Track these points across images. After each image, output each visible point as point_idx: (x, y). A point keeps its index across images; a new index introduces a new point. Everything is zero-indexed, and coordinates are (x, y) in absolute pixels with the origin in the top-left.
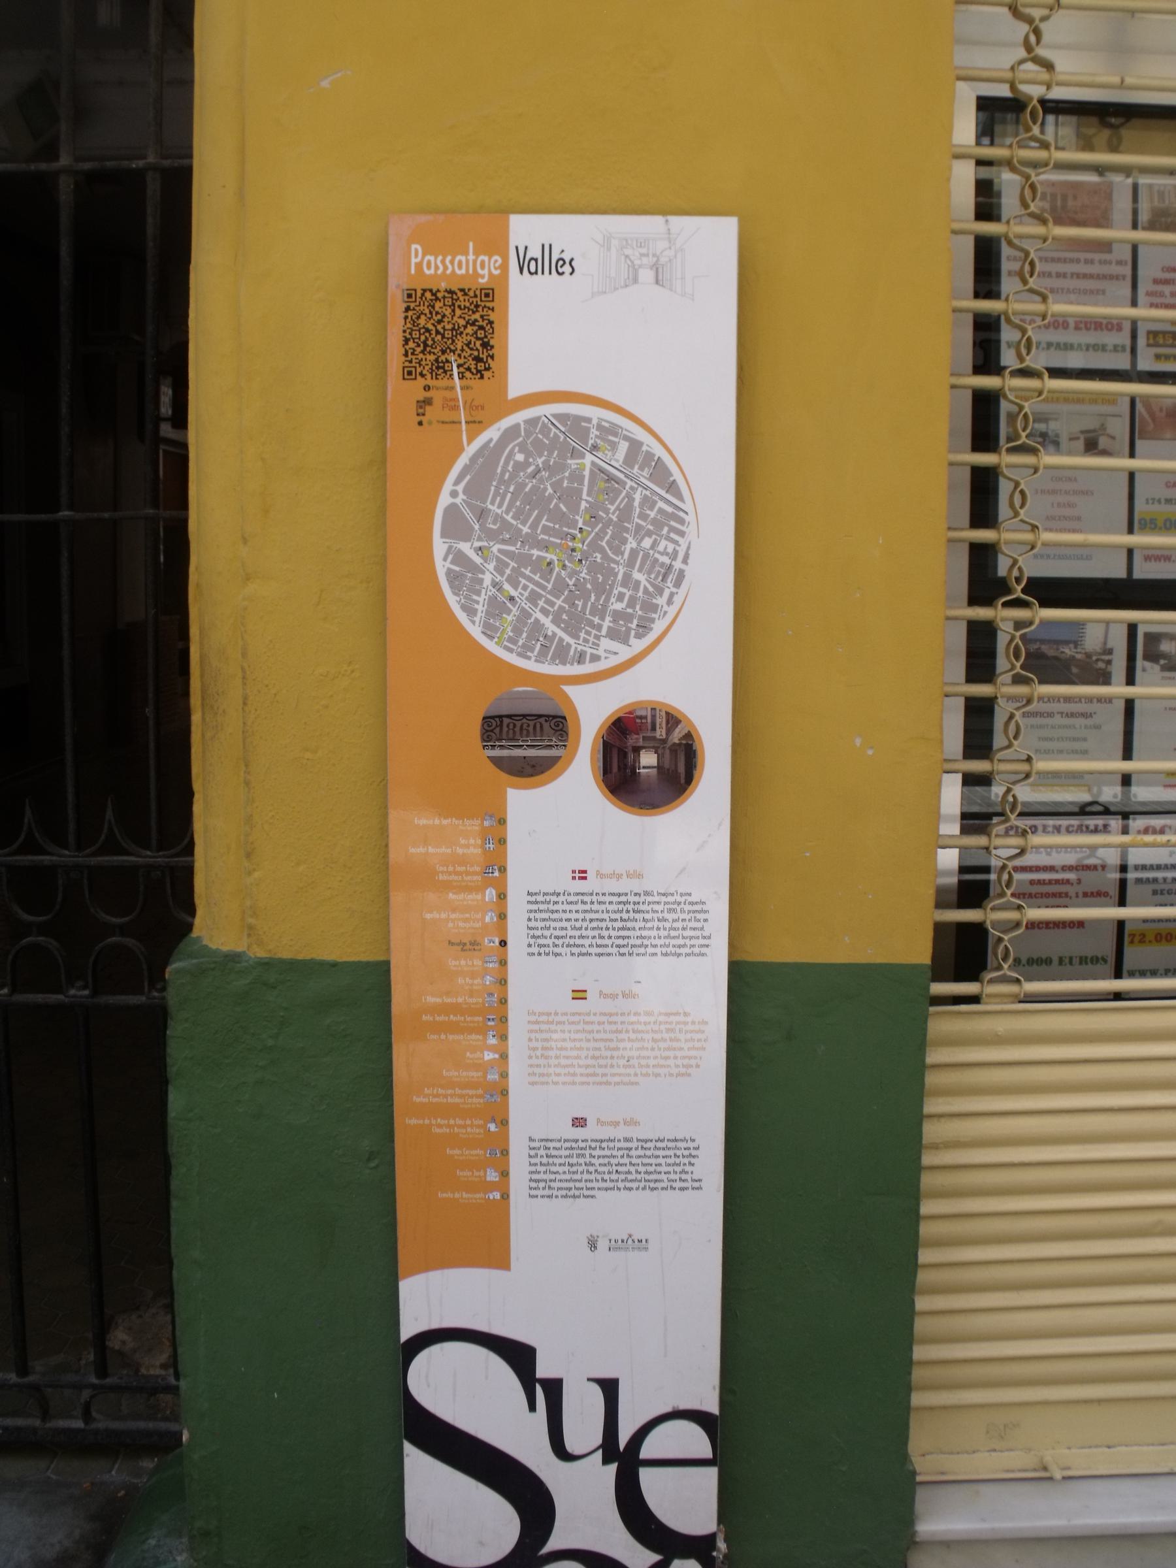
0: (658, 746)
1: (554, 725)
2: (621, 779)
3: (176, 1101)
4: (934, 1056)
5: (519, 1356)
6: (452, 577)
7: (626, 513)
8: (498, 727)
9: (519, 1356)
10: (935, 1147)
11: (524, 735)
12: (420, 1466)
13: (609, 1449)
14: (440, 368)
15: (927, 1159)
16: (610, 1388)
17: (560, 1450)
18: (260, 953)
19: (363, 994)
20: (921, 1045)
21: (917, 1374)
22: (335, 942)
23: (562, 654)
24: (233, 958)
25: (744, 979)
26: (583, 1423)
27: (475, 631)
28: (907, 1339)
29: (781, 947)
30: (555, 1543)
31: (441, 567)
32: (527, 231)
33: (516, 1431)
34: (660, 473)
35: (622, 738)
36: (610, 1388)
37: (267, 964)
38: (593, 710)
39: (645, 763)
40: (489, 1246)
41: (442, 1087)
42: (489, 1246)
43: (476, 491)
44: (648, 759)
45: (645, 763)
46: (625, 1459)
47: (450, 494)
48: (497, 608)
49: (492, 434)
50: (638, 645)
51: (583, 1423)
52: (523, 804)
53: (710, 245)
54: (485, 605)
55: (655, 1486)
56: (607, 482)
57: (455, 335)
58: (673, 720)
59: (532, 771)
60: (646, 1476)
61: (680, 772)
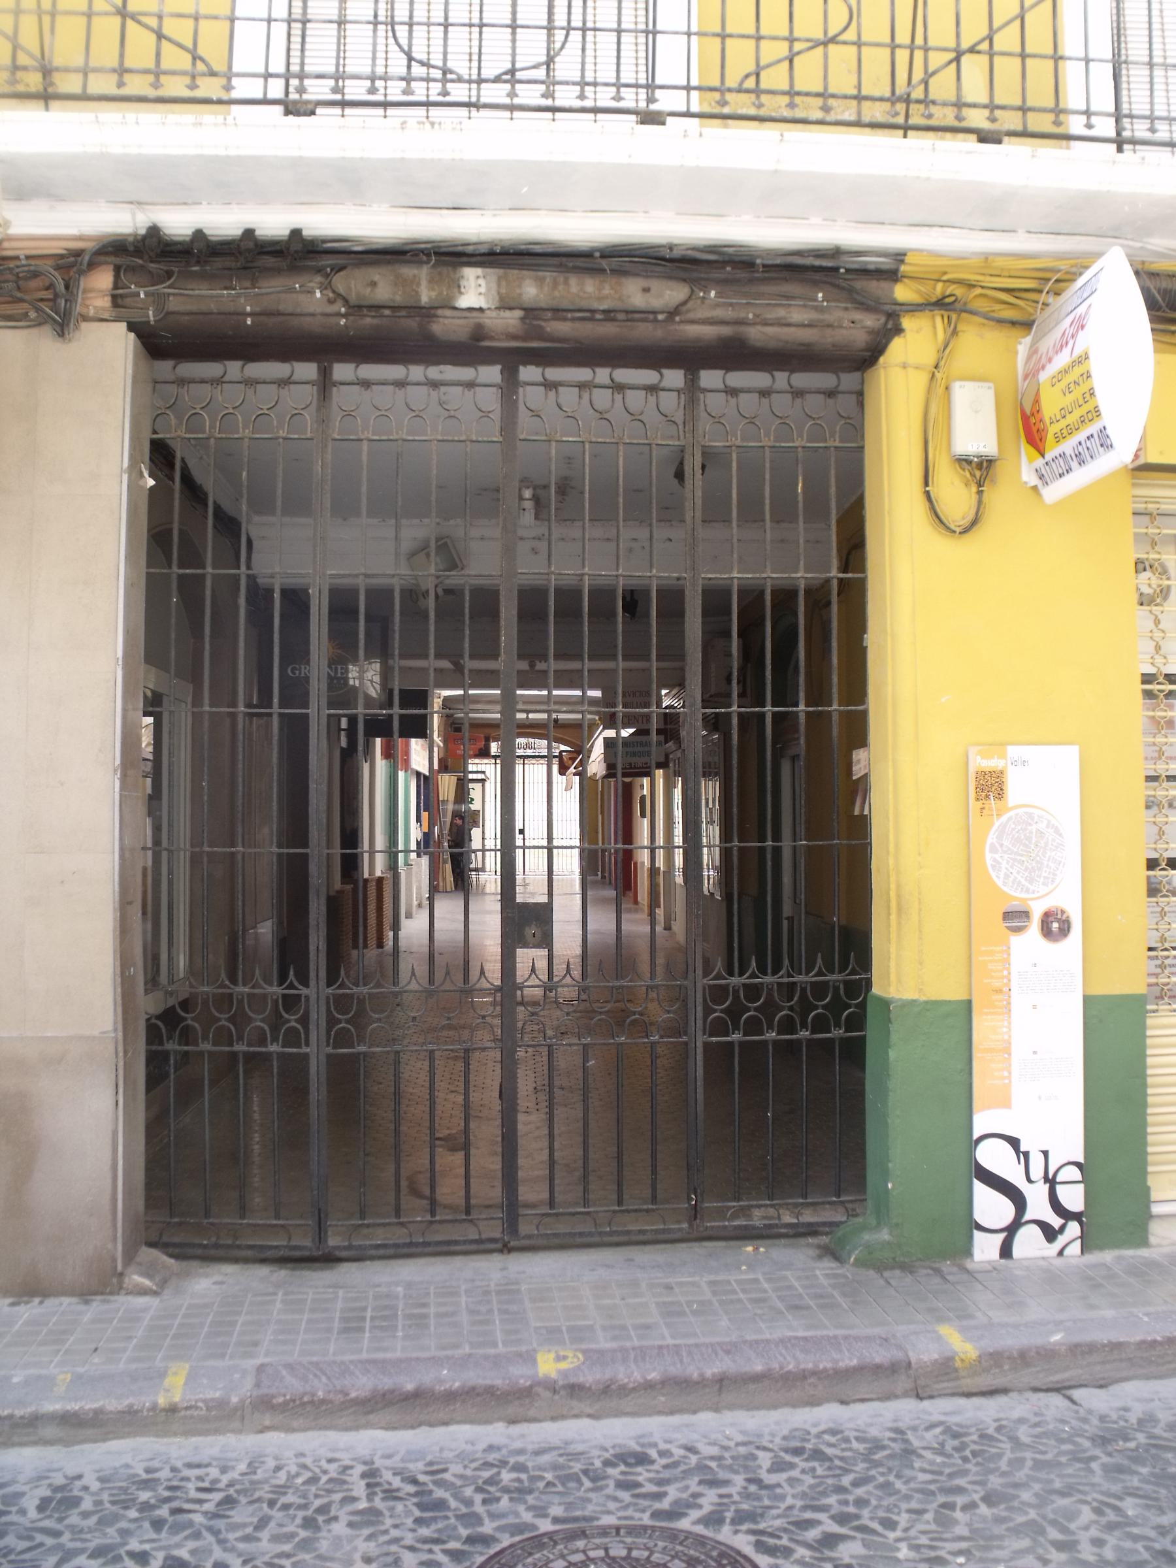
0: (1059, 921)
1: (1026, 914)
2: (1047, 932)
3: (892, 1054)
4: (1149, 1111)
5: (1014, 1142)
6: (993, 867)
7: (1046, 844)
8: (1007, 916)
9: (1014, 1142)
10: (1154, 1145)
11: (1015, 918)
12: (979, 1188)
13: (1046, 1179)
14: (987, 797)
15: (1149, 1130)
16: (1046, 1153)
17: (1029, 1180)
18: (924, 998)
19: (962, 1014)
20: (1144, 1027)
21: (1150, 1158)
22: (949, 991)
23: (1027, 891)
24: (914, 1001)
25: (1088, 1001)
26: (1037, 1171)
27: (999, 883)
28: (1145, 1144)
29: (1098, 990)
30: (1027, 1217)
31: (989, 862)
32: (1013, 751)
33: (1012, 1172)
34: (1057, 831)
35: (1047, 918)
36: (1046, 1153)
37: (926, 1002)
38: (1037, 911)
39: (1054, 926)
40: (1004, 1101)
41: (192, 1417)
42: (1004, 1101)
43: (1000, 837)
44: (1055, 925)
45: (1054, 926)
46: (1051, 1182)
47: (992, 838)
48: (1007, 876)
49: (1004, 818)
50: (1051, 887)
51: (1037, 1171)
52: (1016, 940)
53: (1071, 754)
54: (1007, 876)
55: (1062, 1192)
56: (1040, 833)
57: (991, 786)
58: (1063, 912)
59: (1018, 930)
60: (1059, 1188)
61: (1066, 929)
